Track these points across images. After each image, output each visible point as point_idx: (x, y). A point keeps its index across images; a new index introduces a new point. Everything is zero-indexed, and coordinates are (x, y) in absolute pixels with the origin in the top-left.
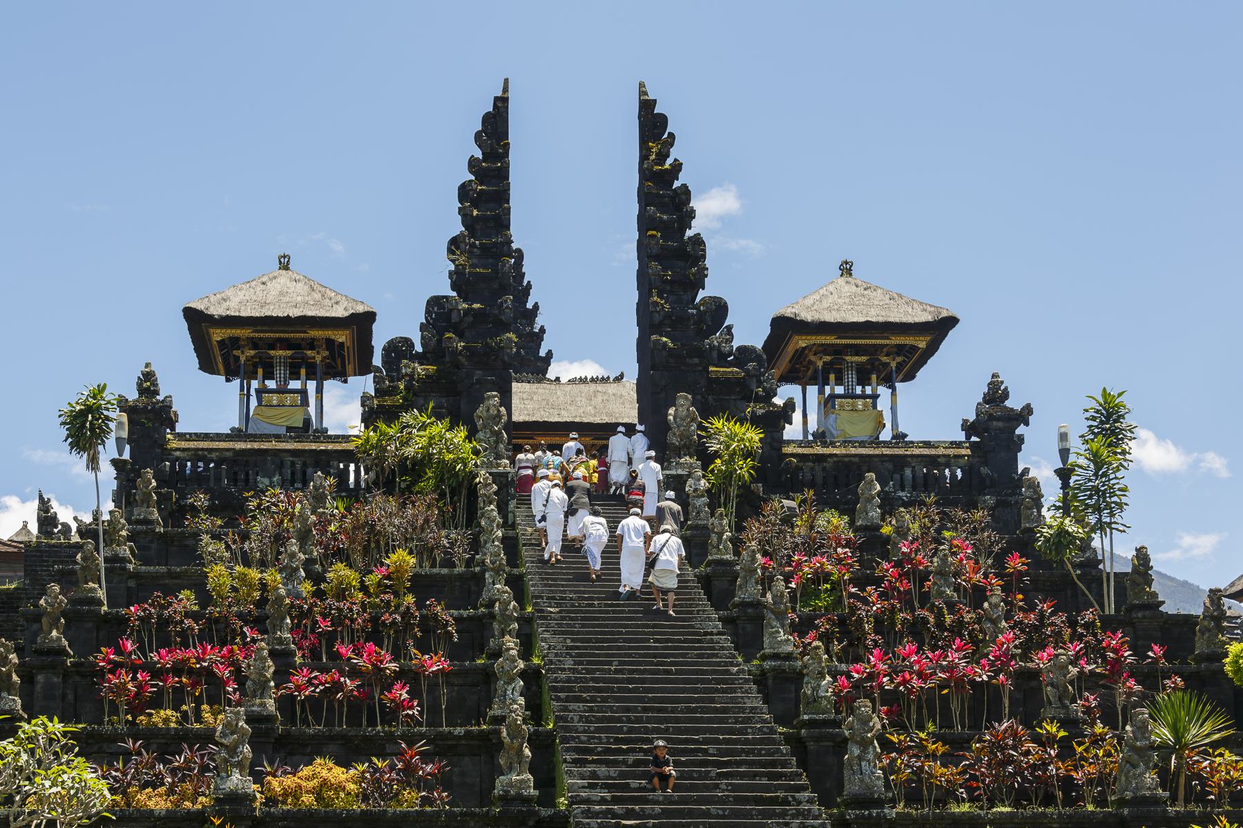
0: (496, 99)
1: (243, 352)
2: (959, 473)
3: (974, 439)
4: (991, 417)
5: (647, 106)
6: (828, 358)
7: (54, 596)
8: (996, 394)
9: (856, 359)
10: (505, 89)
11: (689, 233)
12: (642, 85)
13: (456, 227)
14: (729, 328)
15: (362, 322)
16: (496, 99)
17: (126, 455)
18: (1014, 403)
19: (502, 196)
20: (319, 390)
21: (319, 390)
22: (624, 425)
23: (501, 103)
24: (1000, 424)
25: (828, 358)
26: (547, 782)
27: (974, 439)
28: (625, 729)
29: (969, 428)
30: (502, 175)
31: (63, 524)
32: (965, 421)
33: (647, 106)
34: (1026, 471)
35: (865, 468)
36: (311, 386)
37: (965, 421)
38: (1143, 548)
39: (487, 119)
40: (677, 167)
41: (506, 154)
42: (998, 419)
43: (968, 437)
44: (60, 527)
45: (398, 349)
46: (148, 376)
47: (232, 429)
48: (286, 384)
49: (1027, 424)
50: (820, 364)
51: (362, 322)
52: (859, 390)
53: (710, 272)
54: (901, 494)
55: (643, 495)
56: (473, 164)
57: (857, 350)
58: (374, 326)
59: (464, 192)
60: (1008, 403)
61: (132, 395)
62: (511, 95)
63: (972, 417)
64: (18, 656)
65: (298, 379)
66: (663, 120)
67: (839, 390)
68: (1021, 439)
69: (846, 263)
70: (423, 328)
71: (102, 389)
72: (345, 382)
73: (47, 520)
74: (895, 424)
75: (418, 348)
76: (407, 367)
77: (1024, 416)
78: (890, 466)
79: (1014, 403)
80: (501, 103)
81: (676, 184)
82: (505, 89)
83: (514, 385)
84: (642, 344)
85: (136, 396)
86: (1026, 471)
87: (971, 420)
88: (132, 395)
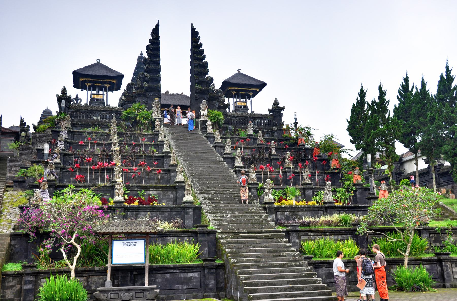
3: (271, 114)
5: (193, 29)
6: (235, 92)
8: (276, 103)
12: (192, 24)
18: (281, 105)
19: (158, 49)
20: (107, 94)
21: (107, 94)
22: (180, 106)
23: (158, 26)
24: (278, 110)
25: (235, 92)
27: (271, 114)
29: (270, 111)
31: (27, 125)
32: (269, 109)
33: (193, 29)
36: (105, 93)
37: (269, 109)
39: (154, 30)
40: (201, 45)
41: (159, 39)
42: (277, 109)
43: (270, 113)
44: (26, 126)
48: (99, 93)
49: (284, 111)
50: (234, 94)
52: (242, 100)
56: (150, 41)
57: (242, 91)
59: (148, 47)
60: (279, 105)
61: (60, 94)
63: (271, 108)
65: (102, 91)
66: (197, 33)
67: (238, 100)
71: (395, 106)
72: (113, 92)
77: (283, 109)
79: (281, 105)
80: (158, 26)
81: (201, 49)
83: (189, 96)
84: (191, 87)
88: (60, 94)
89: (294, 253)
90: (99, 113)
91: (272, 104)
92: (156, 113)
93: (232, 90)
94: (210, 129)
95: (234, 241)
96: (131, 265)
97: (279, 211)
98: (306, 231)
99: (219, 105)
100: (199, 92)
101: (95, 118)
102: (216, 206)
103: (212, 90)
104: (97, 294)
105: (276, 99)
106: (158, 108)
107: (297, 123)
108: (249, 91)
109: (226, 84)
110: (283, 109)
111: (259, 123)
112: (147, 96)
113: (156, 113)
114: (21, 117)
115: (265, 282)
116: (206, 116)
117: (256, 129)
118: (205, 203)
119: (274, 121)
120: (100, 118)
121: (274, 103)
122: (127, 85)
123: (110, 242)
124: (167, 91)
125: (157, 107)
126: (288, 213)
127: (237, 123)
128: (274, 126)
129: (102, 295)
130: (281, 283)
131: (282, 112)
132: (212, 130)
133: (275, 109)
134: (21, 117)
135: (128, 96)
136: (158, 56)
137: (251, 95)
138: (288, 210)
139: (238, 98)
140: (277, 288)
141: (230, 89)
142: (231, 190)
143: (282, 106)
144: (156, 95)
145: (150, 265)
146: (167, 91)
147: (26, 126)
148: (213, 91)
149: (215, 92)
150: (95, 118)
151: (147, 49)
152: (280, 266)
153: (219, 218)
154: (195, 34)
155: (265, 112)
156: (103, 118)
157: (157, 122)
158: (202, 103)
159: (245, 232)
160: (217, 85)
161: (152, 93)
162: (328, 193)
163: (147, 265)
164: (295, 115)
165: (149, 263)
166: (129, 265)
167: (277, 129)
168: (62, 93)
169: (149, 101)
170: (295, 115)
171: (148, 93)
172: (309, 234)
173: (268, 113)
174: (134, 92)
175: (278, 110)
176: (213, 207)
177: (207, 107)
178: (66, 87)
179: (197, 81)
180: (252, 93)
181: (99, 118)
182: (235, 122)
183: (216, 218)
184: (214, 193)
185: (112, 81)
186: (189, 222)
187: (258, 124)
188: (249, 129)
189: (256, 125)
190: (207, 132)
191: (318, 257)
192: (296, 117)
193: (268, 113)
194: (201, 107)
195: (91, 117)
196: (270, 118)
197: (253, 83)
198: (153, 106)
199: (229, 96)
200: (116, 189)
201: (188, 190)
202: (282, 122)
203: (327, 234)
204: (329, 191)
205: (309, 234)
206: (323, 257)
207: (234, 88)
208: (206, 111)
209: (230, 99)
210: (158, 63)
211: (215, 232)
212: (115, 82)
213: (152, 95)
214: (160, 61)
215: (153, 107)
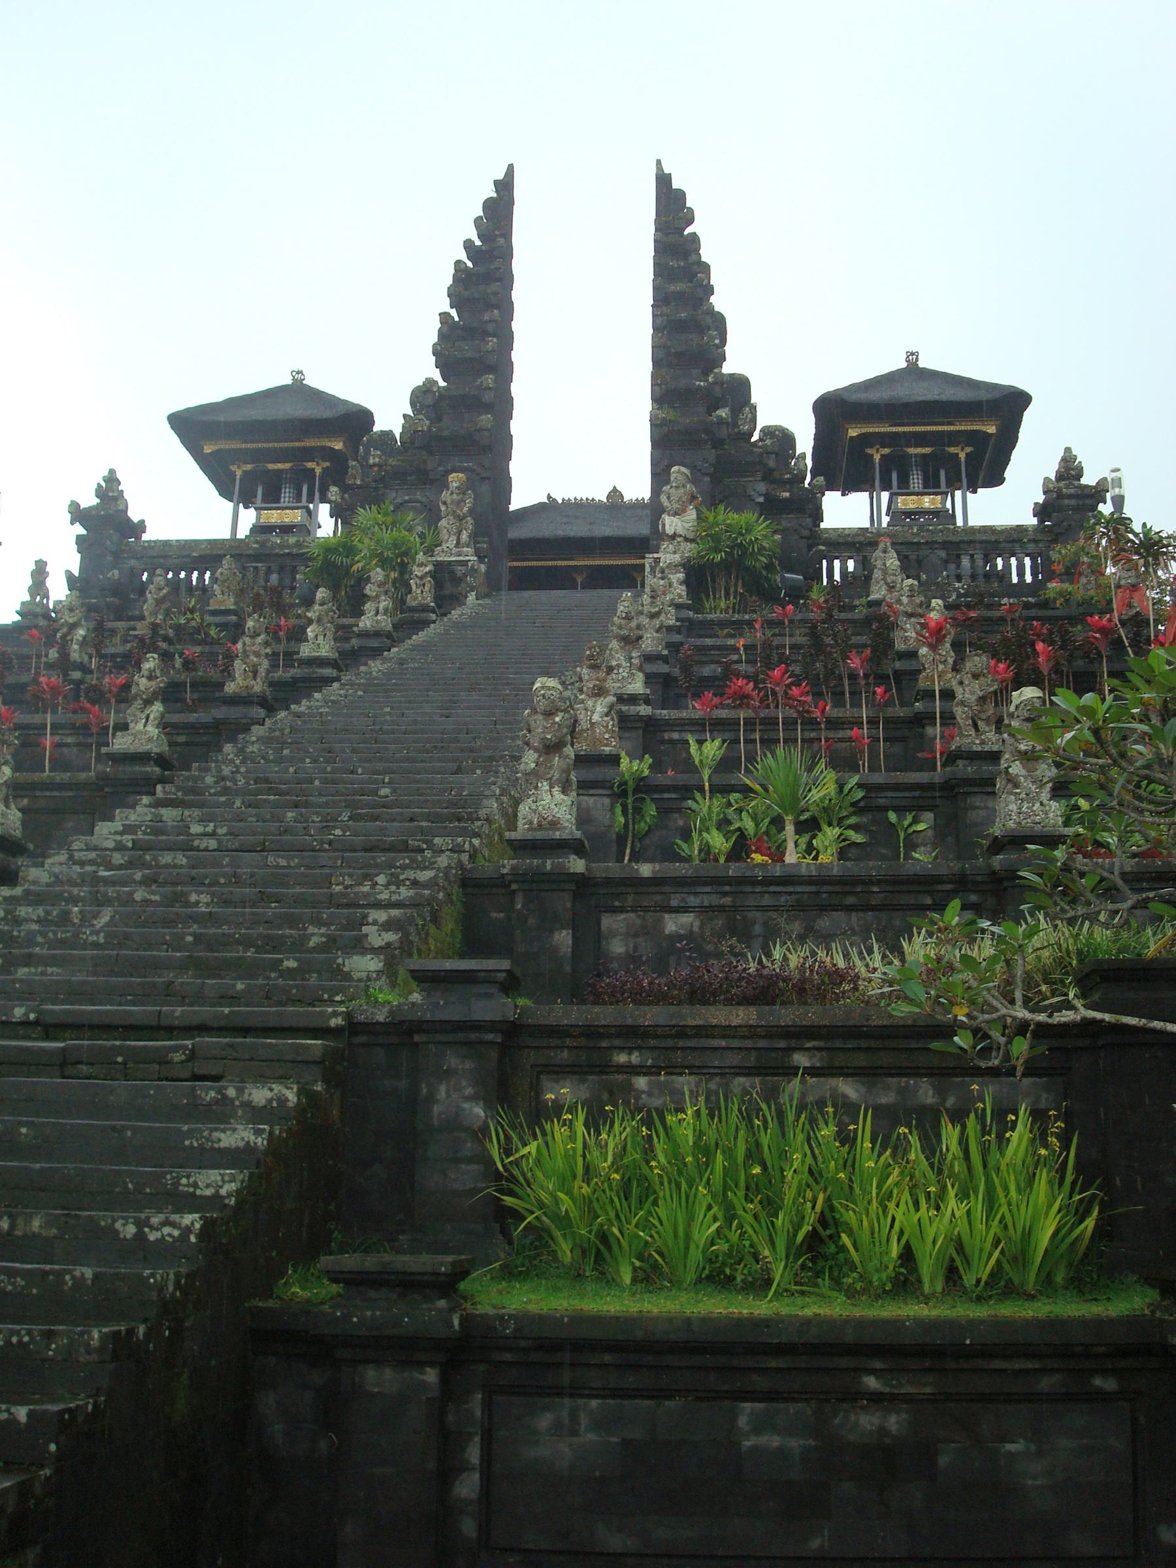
0: (497, 183)
1: (239, 467)
2: (851, 565)
4: (1059, 493)
5: (663, 181)
9: (919, 450)
12: (659, 162)
16: (497, 183)
18: (1089, 479)
23: (505, 186)
24: (1073, 502)
28: (329, 769)
29: (1041, 511)
32: (1036, 504)
33: (663, 181)
37: (1036, 504)
39: (488, 205)
42: (1070, 497)
43: (1041, 521)
46: (112, 479)
54: (957, 585)
55: (582, 588)
60: (1084, 481)
61: (89, 500)
63: (1041, 499)
64: (228, 1205)
66: (681, 195)
69: (912, 354)
78: (943, 554)
79: (1089, 479)
80: (505, 186)
85: (95, 501)
87: (1041, 502)
88: (89, 500)
89: (140, 1224)
93: (866, 440)
97: (622, 910)
98: (591, 1032)
99: (766, 496)
105: (1068, 450)
108: (954, 438)
116: (686, 539)
117: (959, 596)
124: (615, 490)
126: (687, 919)
133: (1060, 495)
135: (359, 487)
137: (962, 456)
138: (693, 901)
141: (853, 433)
142: (384, 791)
146: (615, 490)
159: (25, 1023)
172: (622, 1058)
174: (374, 465)
175: (1073, 502)
177: (693, 498)
178: (119, 476)
180: (969, 449)
185: (329, 444)
189: (966, 580)
191: (627, 1279)
196: (1035, 541)
197: (963, 395)
203: (801, 1060)
205: (622, 1058)
206: (676, 1284)
207: (871, 430)
208: (692, 514)
212: (338, 446)
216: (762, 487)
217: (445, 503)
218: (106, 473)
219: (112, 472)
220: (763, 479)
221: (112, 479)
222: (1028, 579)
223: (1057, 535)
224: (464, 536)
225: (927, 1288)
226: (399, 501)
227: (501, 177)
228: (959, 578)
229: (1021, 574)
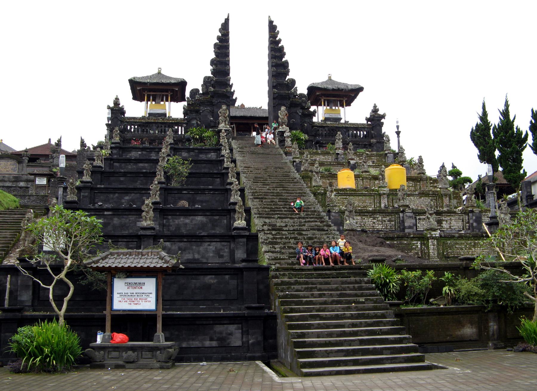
2: (365, 133)
3: (369, 123)
5: (271, 22)
7: (86, 166)
8: (375, 110)
10: (228, 17)
11: (284, 60)
12: (269, 17)
13: (213, 56)
14: (296, 88)
15: (183, 84)
17: (110, 122)
18: (380, 112)
23: (227, 20)
26: (248, 221)
27: (369, 123)
29: (368, 120)
30: (227, 41)
32: (366, 117)
33: (271, 22)
34: (384, 133)
35: (337, 130)
37: (366, 117)
38: (421, 156)
40: (280, 41)
42: (377, 117)
43: (185, 117)
44: (87, 147)
45: (194, 92)
46: (117, 99)
47: (143, 116)
49: (384, 119)
51: (183, 84)
52: (334, 108)
53: (290, 71)
58: (360, 93)
59: (215, 45)
60: (379, 112)
62: (230, 18)
63: (368, 116)
68: (383, 123)
70: (202, 86)
73: (83, 144)
74: (345, 117)
75: (201, 92)
76: (197, 97)
77: (383, 116)
78: (345, 130)
79: (380, 112)
80: (227, 20)
82: (228, 17)
86: (384, 133)
88: (112, 105)
90: (157, 126)
91: (371, 111)
92: (223, 124)
94: (288, 142)
95: (293, 280)
96: (142, 313)
100: (277, 97)
101: (151, 132)
102: (275, 235)
103: (295, 95)
104: (89, 351)
106: (226, 118)
107: (400, 132)
109: (312, 89)
110: (383, 116)
111: (354, 135)
112: (214, 104)
113: (223, 124)
114: (81, 138)
115: (325, 341)
118: (263, 230)
119: (372, 132)
120: (158, 132)
121: (372, 110)
122: (190, 92)
123: (109, 280)
125: (224, 117)
127: (326, 135)
128: (372, 138)
129: (97, 353)
130: (350, 343)
131: (383, 120)
132: (290, 143)
134: (81, 138)
136: (227, 55)
139: (328, 106)
140: (342, 351)
141: (318, 94)
143: (382, 114)
144: (224, 102)
145: (164, 313)
147: (87, 147)
148: (295, 96)
149: (298, 97)
150: (151, 132)
151: (214, 48)
152: (352, 317)
153: (278, 249)
154: (272, 28)
155: (362, 121)
156: (161, 132)
157: (223, 133)
158: (280, 110)
160: (302, 89)
161: (220, 100)
162: (429, 216)
163: (160, 313)
164: (397, 122)
165: (163, 310)
166: (140, 313)
167: (377, 142)
168: (114, 104)
169: (215, 110)
170: (397, 122)
171: (215, 101)
173: (365, 122)
176: (273, 235)
177: (287, 114)
179: (274, 83)
181: (157, 132)
182: (324, 134)
183: (274, 250)
184: (279, 217)
186: (240, 254)
187: (352, 136)
188: (337, 140)
190: (284, 145)
192: (398, 124)
193: (365, 122)
194: (279, 114)
195: (147, 132)
198: (220, 115)
199: (317, 103)
200: (143, 211)
201: (239, 212)
202: (383, 133)
204: (431, 214)
209: (319, 107)
210: (227, 64)
211: (267, 269)
213: (220, 102)
214: (229, 61)
215: (219, 117)
216: (301, 111)
217: (220, 113)
218: (373, 106)
219: (375, 104)
220: (301, 109)
221: (117, 99)
222: (183, 133)
223: (373, 127)
224: (227, 123)
225: (59, 370)
226: (203, 109)
227: (226, 18)
228: (349, 137)
229: (182, 132)
